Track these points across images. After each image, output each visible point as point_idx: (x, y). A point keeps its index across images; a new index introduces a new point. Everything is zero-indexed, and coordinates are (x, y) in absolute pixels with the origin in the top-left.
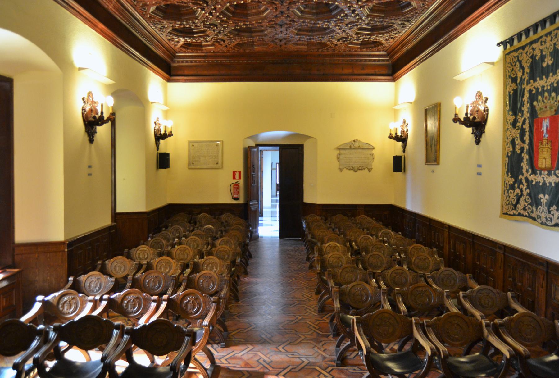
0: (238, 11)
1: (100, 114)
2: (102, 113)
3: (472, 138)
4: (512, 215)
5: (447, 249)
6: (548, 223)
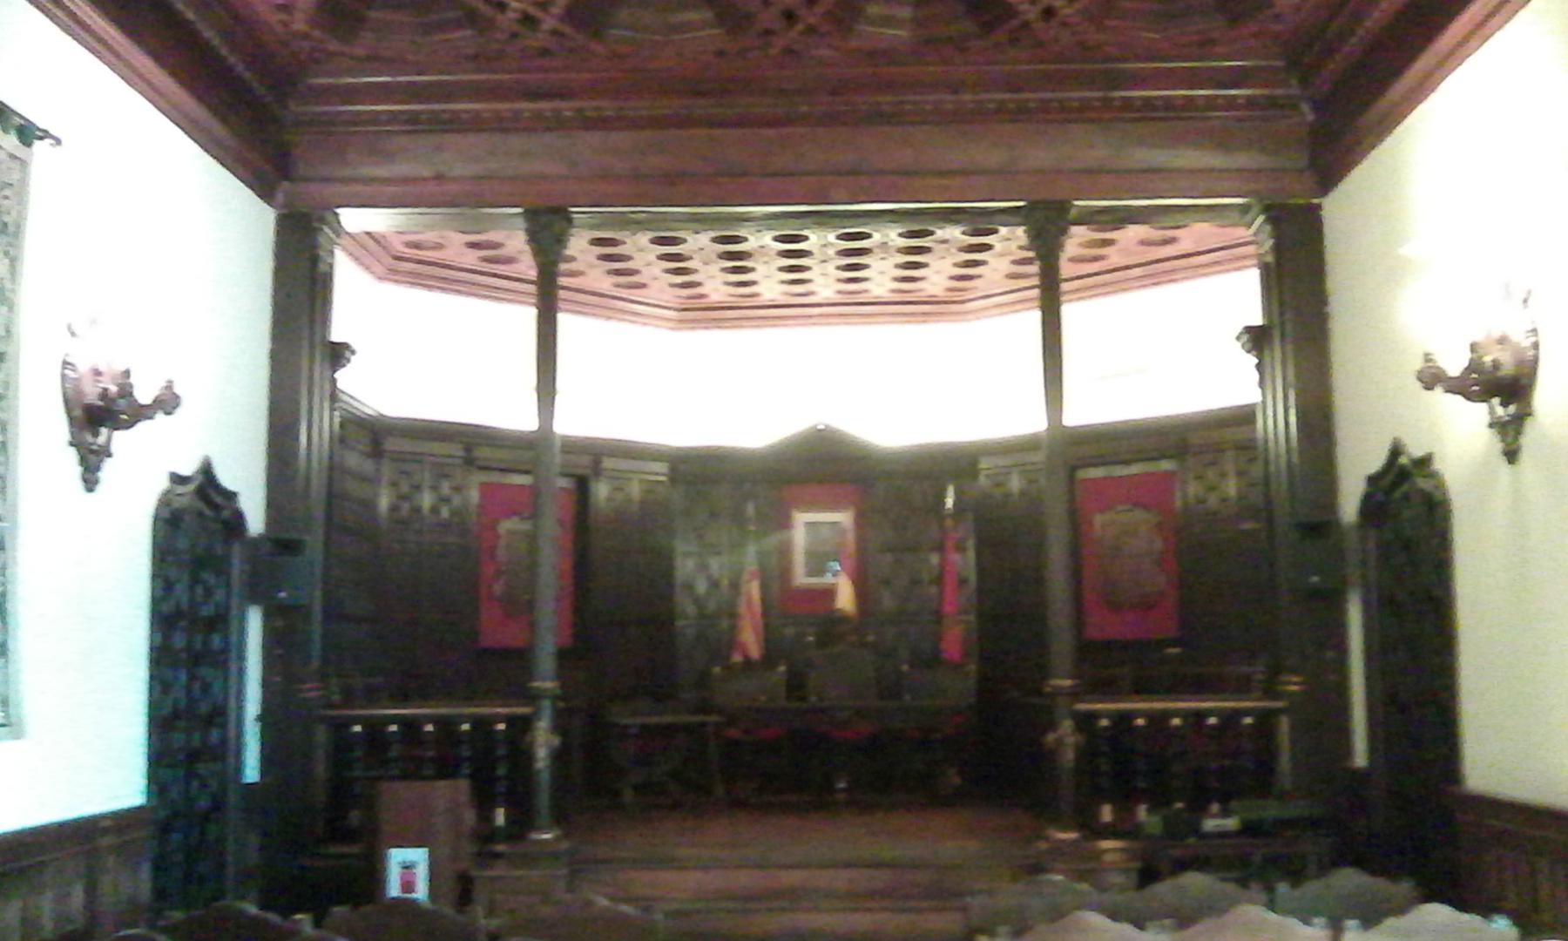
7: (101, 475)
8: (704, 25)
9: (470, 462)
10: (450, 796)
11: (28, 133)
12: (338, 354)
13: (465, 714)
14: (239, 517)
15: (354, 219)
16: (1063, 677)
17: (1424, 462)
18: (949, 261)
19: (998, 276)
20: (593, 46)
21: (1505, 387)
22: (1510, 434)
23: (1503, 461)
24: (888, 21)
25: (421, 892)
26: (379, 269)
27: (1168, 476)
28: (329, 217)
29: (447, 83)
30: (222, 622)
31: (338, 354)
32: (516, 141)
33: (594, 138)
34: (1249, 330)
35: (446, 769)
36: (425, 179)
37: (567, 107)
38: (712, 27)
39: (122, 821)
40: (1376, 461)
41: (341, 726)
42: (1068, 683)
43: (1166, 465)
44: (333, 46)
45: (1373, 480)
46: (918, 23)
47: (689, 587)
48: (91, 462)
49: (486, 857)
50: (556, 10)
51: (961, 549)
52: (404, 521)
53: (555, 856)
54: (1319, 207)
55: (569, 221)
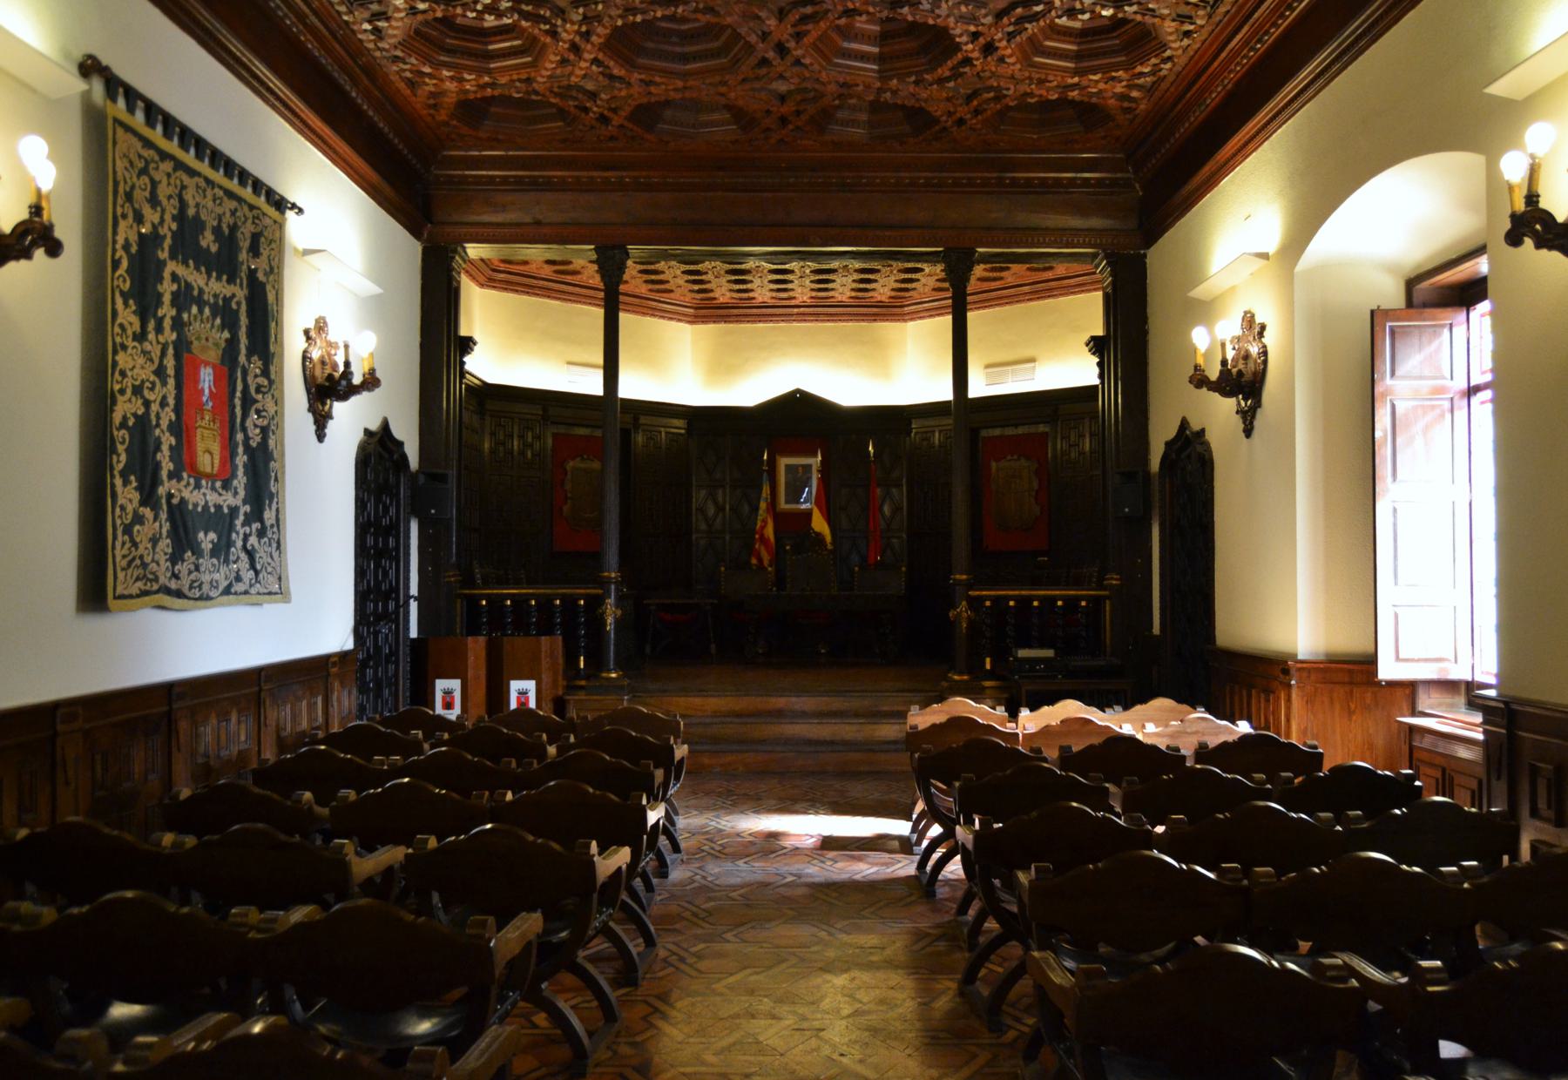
1: (341, 369)
2: (347, 364)
3: (1237, 423)
4: (138, 596)
5: (1294, 695)
6: (203, 184)
10: (550, 646)
11: (281, 204)
13: (557, 595)
14: (404, 457)
15: (474, 251)
22: (1248, 419)
24: (853, 123)
25: (532, 704)
26: (482, 279)
30: (396, 530)
31: (467, 345)
34: (1093, 338)
35: (547, 630)
39: (343, 656)
40: (1171, 433)
41: (472, 601)
43: (1042, 428)
47: (701, 510)
49: (571, 688)
51: (899, 486)
53: (622, 688)
54: (1145, 256)
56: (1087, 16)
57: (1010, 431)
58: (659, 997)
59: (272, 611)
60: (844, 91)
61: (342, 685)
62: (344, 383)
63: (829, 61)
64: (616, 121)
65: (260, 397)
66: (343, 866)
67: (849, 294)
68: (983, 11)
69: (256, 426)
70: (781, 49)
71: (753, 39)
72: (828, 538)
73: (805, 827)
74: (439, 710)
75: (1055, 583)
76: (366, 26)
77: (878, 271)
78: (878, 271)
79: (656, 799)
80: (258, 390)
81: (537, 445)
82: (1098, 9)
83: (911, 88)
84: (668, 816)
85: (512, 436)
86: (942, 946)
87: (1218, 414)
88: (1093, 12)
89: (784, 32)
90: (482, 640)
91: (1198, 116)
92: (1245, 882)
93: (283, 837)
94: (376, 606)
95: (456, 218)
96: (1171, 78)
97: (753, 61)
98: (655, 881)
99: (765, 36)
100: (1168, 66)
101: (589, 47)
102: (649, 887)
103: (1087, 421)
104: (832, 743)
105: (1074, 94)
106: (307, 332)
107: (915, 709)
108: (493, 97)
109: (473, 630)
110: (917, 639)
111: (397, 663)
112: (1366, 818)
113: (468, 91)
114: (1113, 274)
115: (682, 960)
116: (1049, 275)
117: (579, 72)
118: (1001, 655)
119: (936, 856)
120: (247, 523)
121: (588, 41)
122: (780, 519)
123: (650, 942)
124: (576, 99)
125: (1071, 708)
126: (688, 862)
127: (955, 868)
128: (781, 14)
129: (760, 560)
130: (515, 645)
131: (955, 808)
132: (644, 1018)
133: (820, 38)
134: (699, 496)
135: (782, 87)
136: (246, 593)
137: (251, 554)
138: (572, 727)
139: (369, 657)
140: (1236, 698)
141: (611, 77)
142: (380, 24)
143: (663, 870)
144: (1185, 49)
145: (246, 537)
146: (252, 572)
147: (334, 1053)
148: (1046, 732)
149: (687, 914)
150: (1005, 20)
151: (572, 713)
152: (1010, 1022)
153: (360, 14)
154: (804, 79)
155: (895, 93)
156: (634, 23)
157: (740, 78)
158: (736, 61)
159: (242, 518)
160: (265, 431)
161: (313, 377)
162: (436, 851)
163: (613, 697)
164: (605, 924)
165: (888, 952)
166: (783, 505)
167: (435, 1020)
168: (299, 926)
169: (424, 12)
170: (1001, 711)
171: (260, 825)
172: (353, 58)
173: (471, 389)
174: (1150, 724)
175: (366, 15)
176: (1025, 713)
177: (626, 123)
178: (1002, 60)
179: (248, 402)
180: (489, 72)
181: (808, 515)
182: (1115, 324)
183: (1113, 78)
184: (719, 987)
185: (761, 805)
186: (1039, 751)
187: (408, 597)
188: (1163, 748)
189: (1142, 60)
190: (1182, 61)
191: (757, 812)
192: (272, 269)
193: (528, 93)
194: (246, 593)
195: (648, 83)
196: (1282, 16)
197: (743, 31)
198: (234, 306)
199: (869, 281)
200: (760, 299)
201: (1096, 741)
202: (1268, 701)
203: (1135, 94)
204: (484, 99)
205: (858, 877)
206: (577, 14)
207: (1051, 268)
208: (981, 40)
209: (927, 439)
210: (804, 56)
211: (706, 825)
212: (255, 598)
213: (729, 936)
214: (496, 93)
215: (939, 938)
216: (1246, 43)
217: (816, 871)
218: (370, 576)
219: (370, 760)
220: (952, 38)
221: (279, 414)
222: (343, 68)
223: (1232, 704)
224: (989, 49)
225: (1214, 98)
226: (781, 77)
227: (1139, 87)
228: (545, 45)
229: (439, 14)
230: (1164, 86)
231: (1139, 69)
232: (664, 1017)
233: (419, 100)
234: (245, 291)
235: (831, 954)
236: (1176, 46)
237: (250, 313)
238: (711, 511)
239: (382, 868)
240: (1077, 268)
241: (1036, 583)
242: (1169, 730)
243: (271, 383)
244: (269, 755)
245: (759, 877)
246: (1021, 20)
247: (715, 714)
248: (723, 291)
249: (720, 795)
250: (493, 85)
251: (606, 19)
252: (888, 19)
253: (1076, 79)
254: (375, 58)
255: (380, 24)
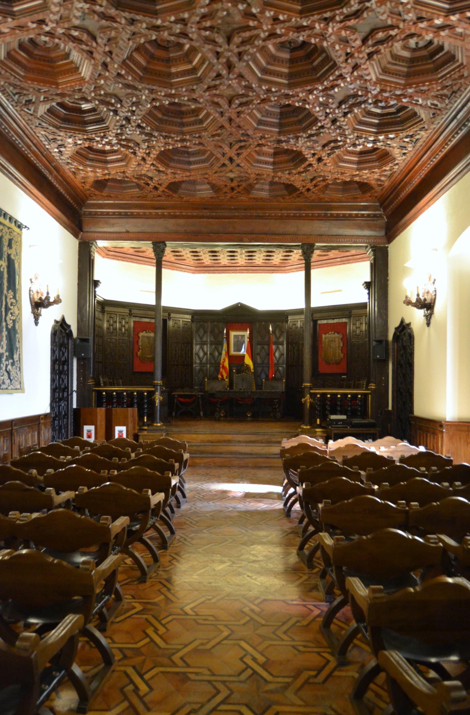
0: (152, 67)
2: (48, 293)
7: (39, 321)
8: (207, 190)
9: (130, 314)
10: (132, 412)
11: (20, 226)
12: (96, 283)
13: (135, 389)
14: (71, 332)
15: (101, 243)
16: (307, 382)
17: (409, 324)
18: (280, 255)
19: (296, 260)
20: (174, 195)
21: (427, 306)
22: (428, 318)
23: (426, 326)
24: (262, 190)
25: (125, 436)
26: (103, 254)
27: (345, 324)
28: (94, 243)
29: (130, 204)
31: (96, 283)
32: (151, 221)
33: (173, 221)
34: (366, 283)
36: (123, 232)
37: (166, 212)
38: (209, 190)
40: (397, 324)
42: (309, 384)
43: (344, 320)
44: (97, 192)
45: (397, 329)
46: (270, 191)
47: (197, 354)
48: (37, 317)
49: (141, 430)
50: (164, 186)
51: (282, 344)
52: (112, 331)
53: (162, 430)
54: (388, 247)
55: (166, 245)
56: (361, 147)
57: (331, 321)
58: (176, 554)
59: (17, 396)
60: (258, 177)
61: (45, 427)
62: (46, 301)
63: (251, 164)
64: (161, 189)
65: (12, 307)
66: (50, 499)
67: (262, 261)
68: (317, 145)
69: (11, 319)
70: (231, 160)
71: (219, 156)
72: (252, 367)
73: (239, 488)
74: (85, 438)
75: (349, 387)
76: (56, 150)
77: (274, 252)
78: (274, 252)
79: (176, 475)
80: (11, 305)
81: (127, 326)
82: (366, 144)
83: (287, 176)
84: (180, 482)
85: (116, 322)
86: (291, 536)
87: (417, 317)
88: (364, 145)
89: (232, 153)
90: (103, 409)
91: (409, 189)
92: (407, 508)
93: (27, 487)
94: (59, 395)
95: (93, 229)
96: (399, 172)
97: (219, 165)
98: (175, 509)
99: (224, 155)
100: (397, 167)
101: (150, 159)
102: (173, 512)
103: (364, 317)
104: (251, 454)
105: (357, 179)
106: (31, 280)
107: (285, 440)
108: (109, 179)
109: (99, 404)
110: (287, 409)
111: (68, 418)
112: (463, 484)
113: (98, 177)
114: (375, 255)
115: (185, 540)
116: (348, 254)
117: (145, 169)
118: (324, 418)
119: (291, 501)
120: (7, 360)
121: (149, 156)
122: (231, 358)
123: (173, 532)
124: (144, 180)
125: (350, 440)
126: (189, 502)
127: (297, 506)
128: (231, 145)
129: (222, 376)
130: (118, 411)
131: (298, 480)
132: (170, 561)
133: (247, 155)
134: (196, 348)
135: (231, 175)
136: (7, 389)
137: (8, 373)
138: (141, 446)
139: (56, 416)
140: (421, 437)
141: (159, 171)
142: (62, 149)
143: (178, 505)
144: (404, 160)
145: (7, 366)
146: (9, 380)
147: (53, 560)
148: (339, 450)
149: (188, 522)
150: (326, 148)
151: (141, 440)
152: (317, 565)
153: (54, 145)
154: (241, 172)
155: (280, 178)
156: (169, 150)
157: (214, 171)
158: (212, 165)
159: (5, 358)
160: (14, 321)
161: (34, 298)
162: (87, 493)
163: (157, 433)
164: (154, 523)
165: (269, 538)
166: (232, 352)
167: (50, 641)
168: (36, 519)
169: (80, 144)
170: (321, 441)
171: (18, 482)
172: (51, 164)
173: (99, 302)
174: (386, 448)
175: (56, 145)
176: (331, 442)
177: (165, 190)
178: (325, 164)
179: (7, 309)
180: (107, 169)
181: (243, 357)
182: (375, 276)
183: (373, 172)
184: (200, 550)
185: (220, 479)
186: (334, 457)
187: (72, 392)
188: (386, 457)
189: (386, 164)
190: (403, 165)
191: (219, 482)
192: (17, 253)
193: (124, 177)
194: (7, 389)
195: (174, 174)
196: (444, 148)
197: (215, 152)
198: (2, 270)
199: (270, 256)
200: (223, 263)
201: (358, 454)
202: (434, 438)
203: (383, 178)
204: (105, 180)
205: (259, 509)
206: (144, 146)
207: (349, 251)
208: (316, 156)
209: (295, 325)
210: (241, 163)
211: (197, 487)
212: (10, 391)
213: (204, 531)
214: (110, 177)
215: (290, 533)
216: (429, 158)
217: (241, 506)
218: (57, 382)
219: (59, 458)
220: (304, 156)
221: (20, 314)
222: (46, 168)
223: (420, 438)
224: (320, 160)
225: (416, 181)
226: (231, 171)
227: (385, 176)
228: (131, 158)
229: (87, 145)
230: (395, 175)
231: (384, 168)
232: (178, 561)
233: (77, 181)
234: (6, 263)
235: (246, 538)
236: (400, 159)
237: (9, 272)
238: (201, 354)
239: (66, 499)
240: (359, 251)
241: (341, 387)
242: (390, 450)
243: (16, 301)
244: (16, 456)
245: (218, 508)
246: (333, 148)
247: (202, 441)
248: (207, 259)
249: (203, 475)
250: (109, 174)
251: (157, 148)
252: (276, 148)
253: (357, 173)
254: (59, 163)
255: (62, 149)
